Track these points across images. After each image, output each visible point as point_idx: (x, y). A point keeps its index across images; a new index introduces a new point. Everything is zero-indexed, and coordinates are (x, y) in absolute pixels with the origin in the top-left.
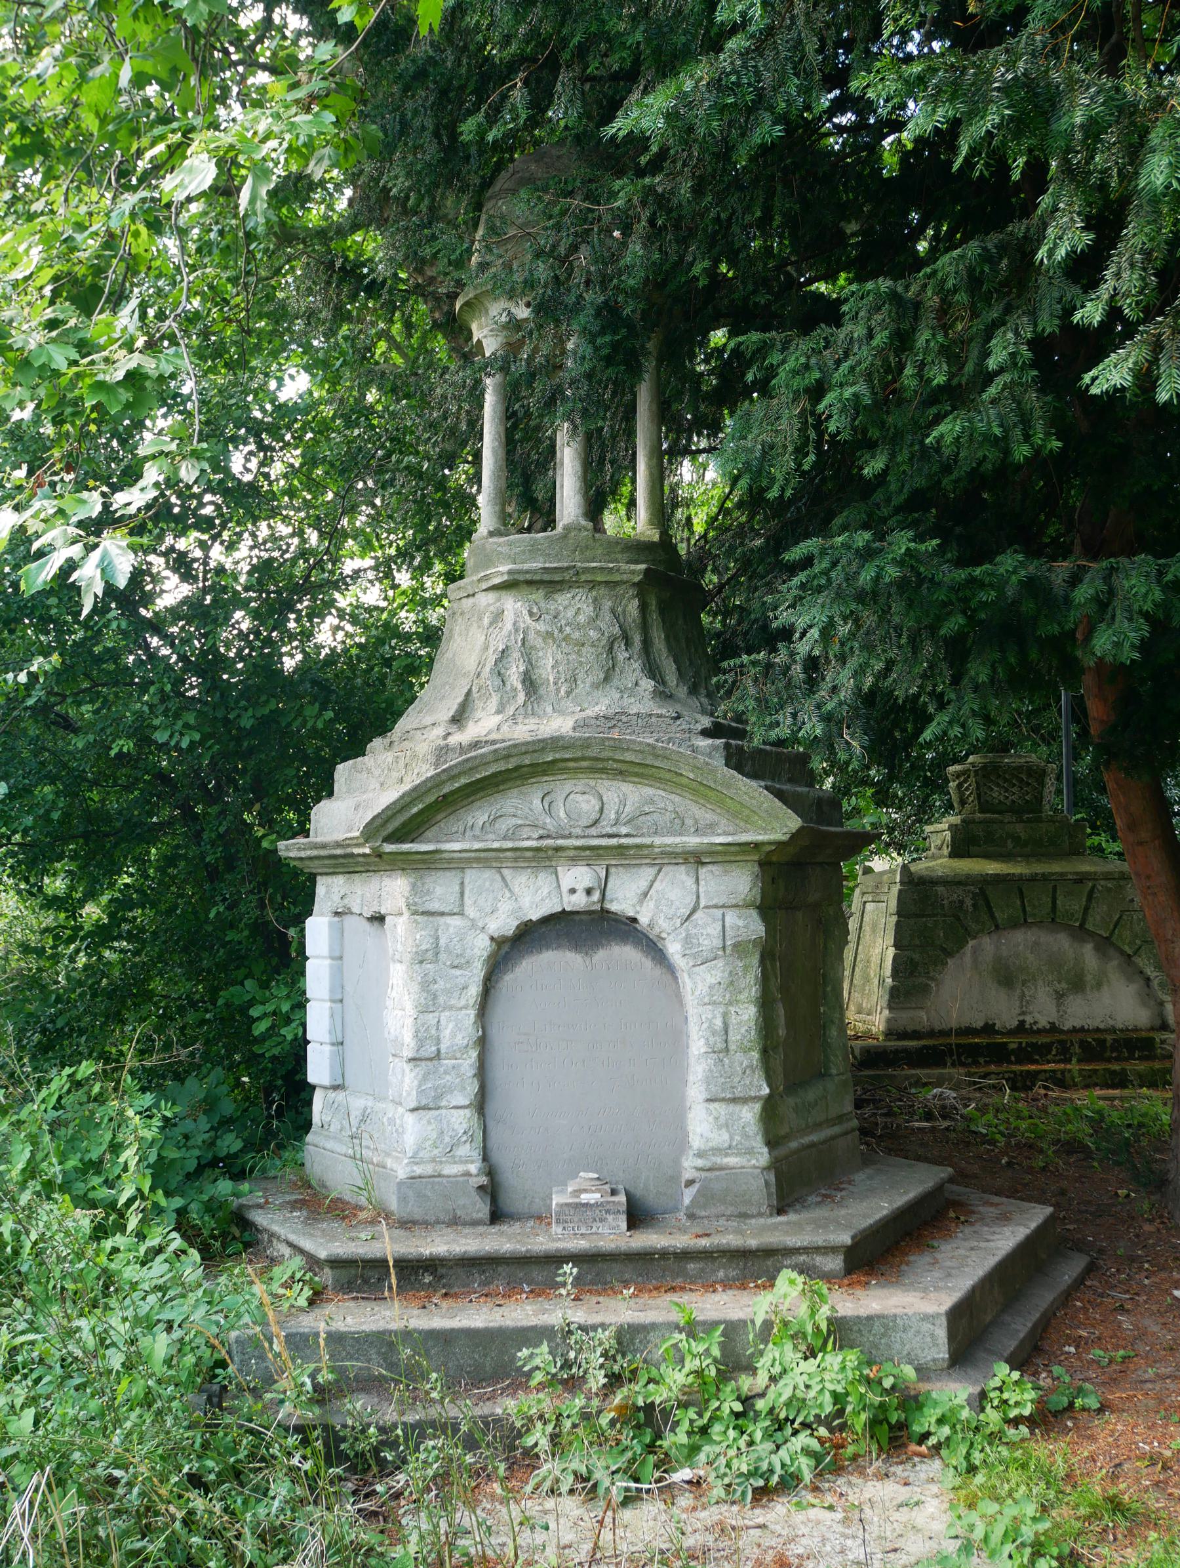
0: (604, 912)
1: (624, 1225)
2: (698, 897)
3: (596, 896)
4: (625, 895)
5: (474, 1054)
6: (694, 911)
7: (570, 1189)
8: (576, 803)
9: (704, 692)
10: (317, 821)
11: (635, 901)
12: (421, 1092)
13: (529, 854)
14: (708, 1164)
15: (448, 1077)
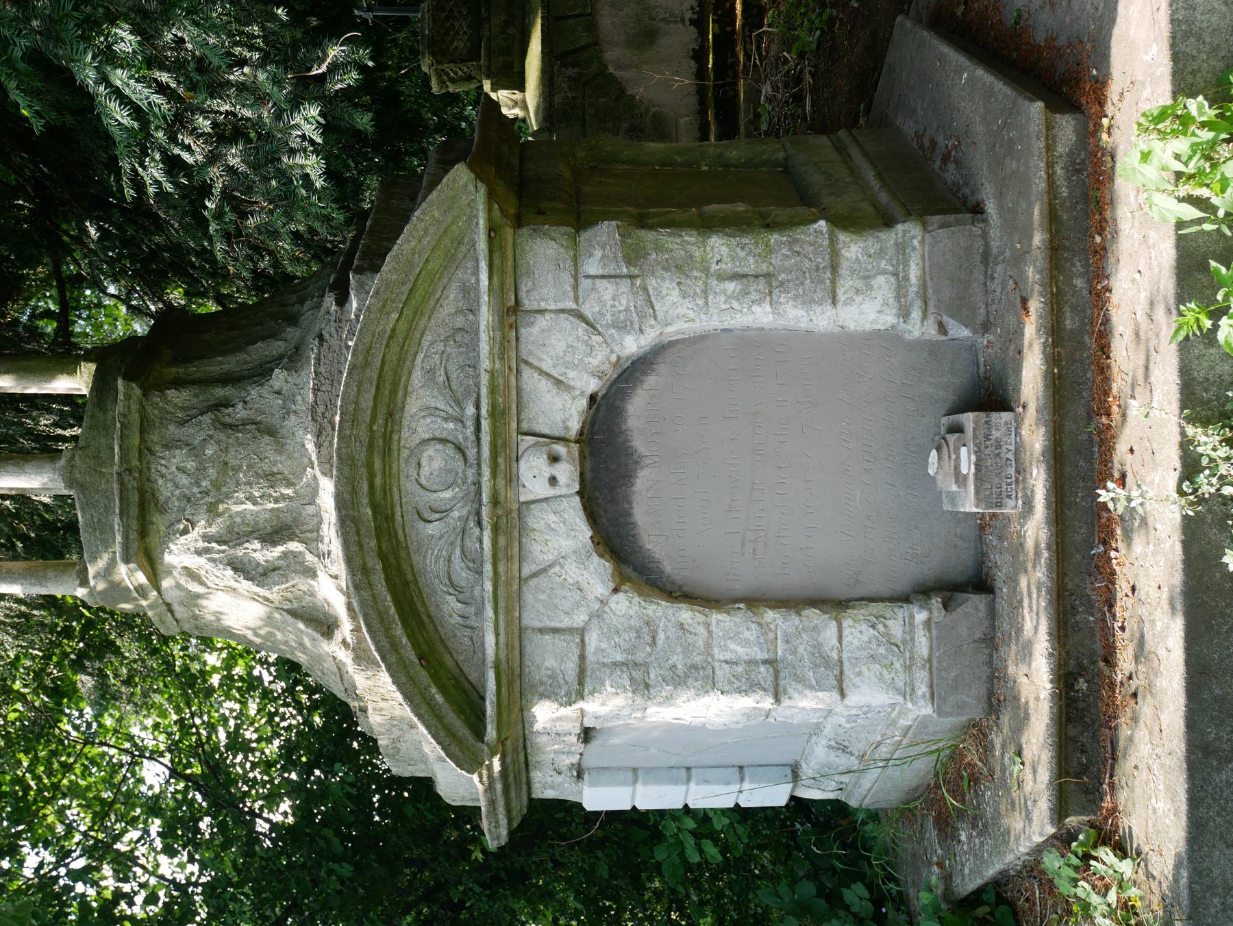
0: (581, 439)
1: (1006, 416)
2: (562, 311)
3: (560, 449)
4: (561, 411)
5: (770, 615)
6: (581, 317)
7: (954, 488)
8: (430, 473)
9: (297, 307)
10: (463, 799)
11: (566, 396)
12: (819, 686)
13: (502, 541)
14: (918, 303)
15: (801, 649)
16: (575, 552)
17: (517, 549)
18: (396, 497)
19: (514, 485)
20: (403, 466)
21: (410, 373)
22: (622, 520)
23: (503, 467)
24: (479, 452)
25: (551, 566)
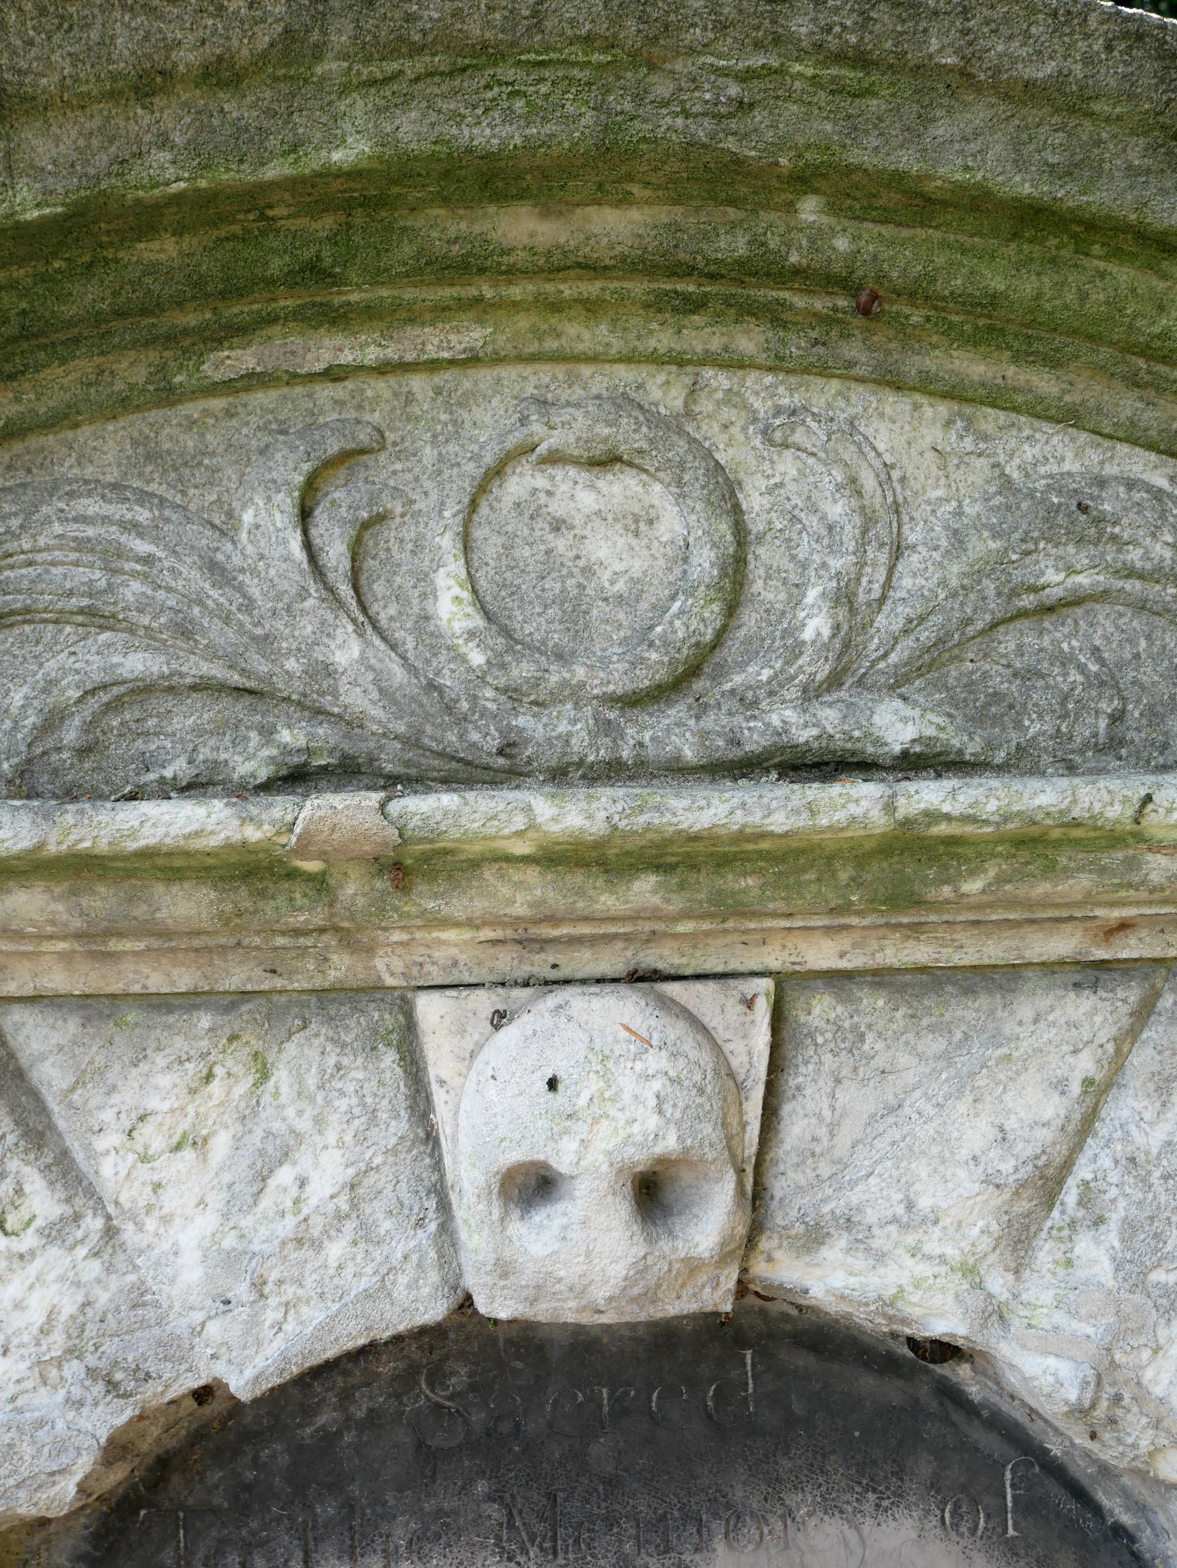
3: (709, 1224)
13: (184, 905)
16: (139, 1297)
17: (155, 982)
18: (435, 341)
19: (506, 962)
20: (598, 380)
21: (1069, 417)
22: (327, 1510)
23: (607, 902)
24: (677, 771)
25: (68, 1174)
